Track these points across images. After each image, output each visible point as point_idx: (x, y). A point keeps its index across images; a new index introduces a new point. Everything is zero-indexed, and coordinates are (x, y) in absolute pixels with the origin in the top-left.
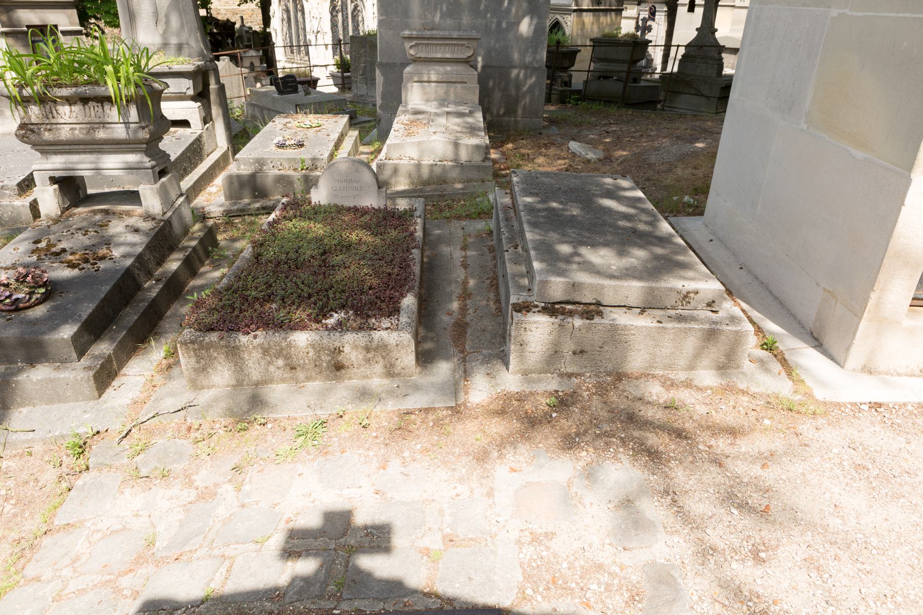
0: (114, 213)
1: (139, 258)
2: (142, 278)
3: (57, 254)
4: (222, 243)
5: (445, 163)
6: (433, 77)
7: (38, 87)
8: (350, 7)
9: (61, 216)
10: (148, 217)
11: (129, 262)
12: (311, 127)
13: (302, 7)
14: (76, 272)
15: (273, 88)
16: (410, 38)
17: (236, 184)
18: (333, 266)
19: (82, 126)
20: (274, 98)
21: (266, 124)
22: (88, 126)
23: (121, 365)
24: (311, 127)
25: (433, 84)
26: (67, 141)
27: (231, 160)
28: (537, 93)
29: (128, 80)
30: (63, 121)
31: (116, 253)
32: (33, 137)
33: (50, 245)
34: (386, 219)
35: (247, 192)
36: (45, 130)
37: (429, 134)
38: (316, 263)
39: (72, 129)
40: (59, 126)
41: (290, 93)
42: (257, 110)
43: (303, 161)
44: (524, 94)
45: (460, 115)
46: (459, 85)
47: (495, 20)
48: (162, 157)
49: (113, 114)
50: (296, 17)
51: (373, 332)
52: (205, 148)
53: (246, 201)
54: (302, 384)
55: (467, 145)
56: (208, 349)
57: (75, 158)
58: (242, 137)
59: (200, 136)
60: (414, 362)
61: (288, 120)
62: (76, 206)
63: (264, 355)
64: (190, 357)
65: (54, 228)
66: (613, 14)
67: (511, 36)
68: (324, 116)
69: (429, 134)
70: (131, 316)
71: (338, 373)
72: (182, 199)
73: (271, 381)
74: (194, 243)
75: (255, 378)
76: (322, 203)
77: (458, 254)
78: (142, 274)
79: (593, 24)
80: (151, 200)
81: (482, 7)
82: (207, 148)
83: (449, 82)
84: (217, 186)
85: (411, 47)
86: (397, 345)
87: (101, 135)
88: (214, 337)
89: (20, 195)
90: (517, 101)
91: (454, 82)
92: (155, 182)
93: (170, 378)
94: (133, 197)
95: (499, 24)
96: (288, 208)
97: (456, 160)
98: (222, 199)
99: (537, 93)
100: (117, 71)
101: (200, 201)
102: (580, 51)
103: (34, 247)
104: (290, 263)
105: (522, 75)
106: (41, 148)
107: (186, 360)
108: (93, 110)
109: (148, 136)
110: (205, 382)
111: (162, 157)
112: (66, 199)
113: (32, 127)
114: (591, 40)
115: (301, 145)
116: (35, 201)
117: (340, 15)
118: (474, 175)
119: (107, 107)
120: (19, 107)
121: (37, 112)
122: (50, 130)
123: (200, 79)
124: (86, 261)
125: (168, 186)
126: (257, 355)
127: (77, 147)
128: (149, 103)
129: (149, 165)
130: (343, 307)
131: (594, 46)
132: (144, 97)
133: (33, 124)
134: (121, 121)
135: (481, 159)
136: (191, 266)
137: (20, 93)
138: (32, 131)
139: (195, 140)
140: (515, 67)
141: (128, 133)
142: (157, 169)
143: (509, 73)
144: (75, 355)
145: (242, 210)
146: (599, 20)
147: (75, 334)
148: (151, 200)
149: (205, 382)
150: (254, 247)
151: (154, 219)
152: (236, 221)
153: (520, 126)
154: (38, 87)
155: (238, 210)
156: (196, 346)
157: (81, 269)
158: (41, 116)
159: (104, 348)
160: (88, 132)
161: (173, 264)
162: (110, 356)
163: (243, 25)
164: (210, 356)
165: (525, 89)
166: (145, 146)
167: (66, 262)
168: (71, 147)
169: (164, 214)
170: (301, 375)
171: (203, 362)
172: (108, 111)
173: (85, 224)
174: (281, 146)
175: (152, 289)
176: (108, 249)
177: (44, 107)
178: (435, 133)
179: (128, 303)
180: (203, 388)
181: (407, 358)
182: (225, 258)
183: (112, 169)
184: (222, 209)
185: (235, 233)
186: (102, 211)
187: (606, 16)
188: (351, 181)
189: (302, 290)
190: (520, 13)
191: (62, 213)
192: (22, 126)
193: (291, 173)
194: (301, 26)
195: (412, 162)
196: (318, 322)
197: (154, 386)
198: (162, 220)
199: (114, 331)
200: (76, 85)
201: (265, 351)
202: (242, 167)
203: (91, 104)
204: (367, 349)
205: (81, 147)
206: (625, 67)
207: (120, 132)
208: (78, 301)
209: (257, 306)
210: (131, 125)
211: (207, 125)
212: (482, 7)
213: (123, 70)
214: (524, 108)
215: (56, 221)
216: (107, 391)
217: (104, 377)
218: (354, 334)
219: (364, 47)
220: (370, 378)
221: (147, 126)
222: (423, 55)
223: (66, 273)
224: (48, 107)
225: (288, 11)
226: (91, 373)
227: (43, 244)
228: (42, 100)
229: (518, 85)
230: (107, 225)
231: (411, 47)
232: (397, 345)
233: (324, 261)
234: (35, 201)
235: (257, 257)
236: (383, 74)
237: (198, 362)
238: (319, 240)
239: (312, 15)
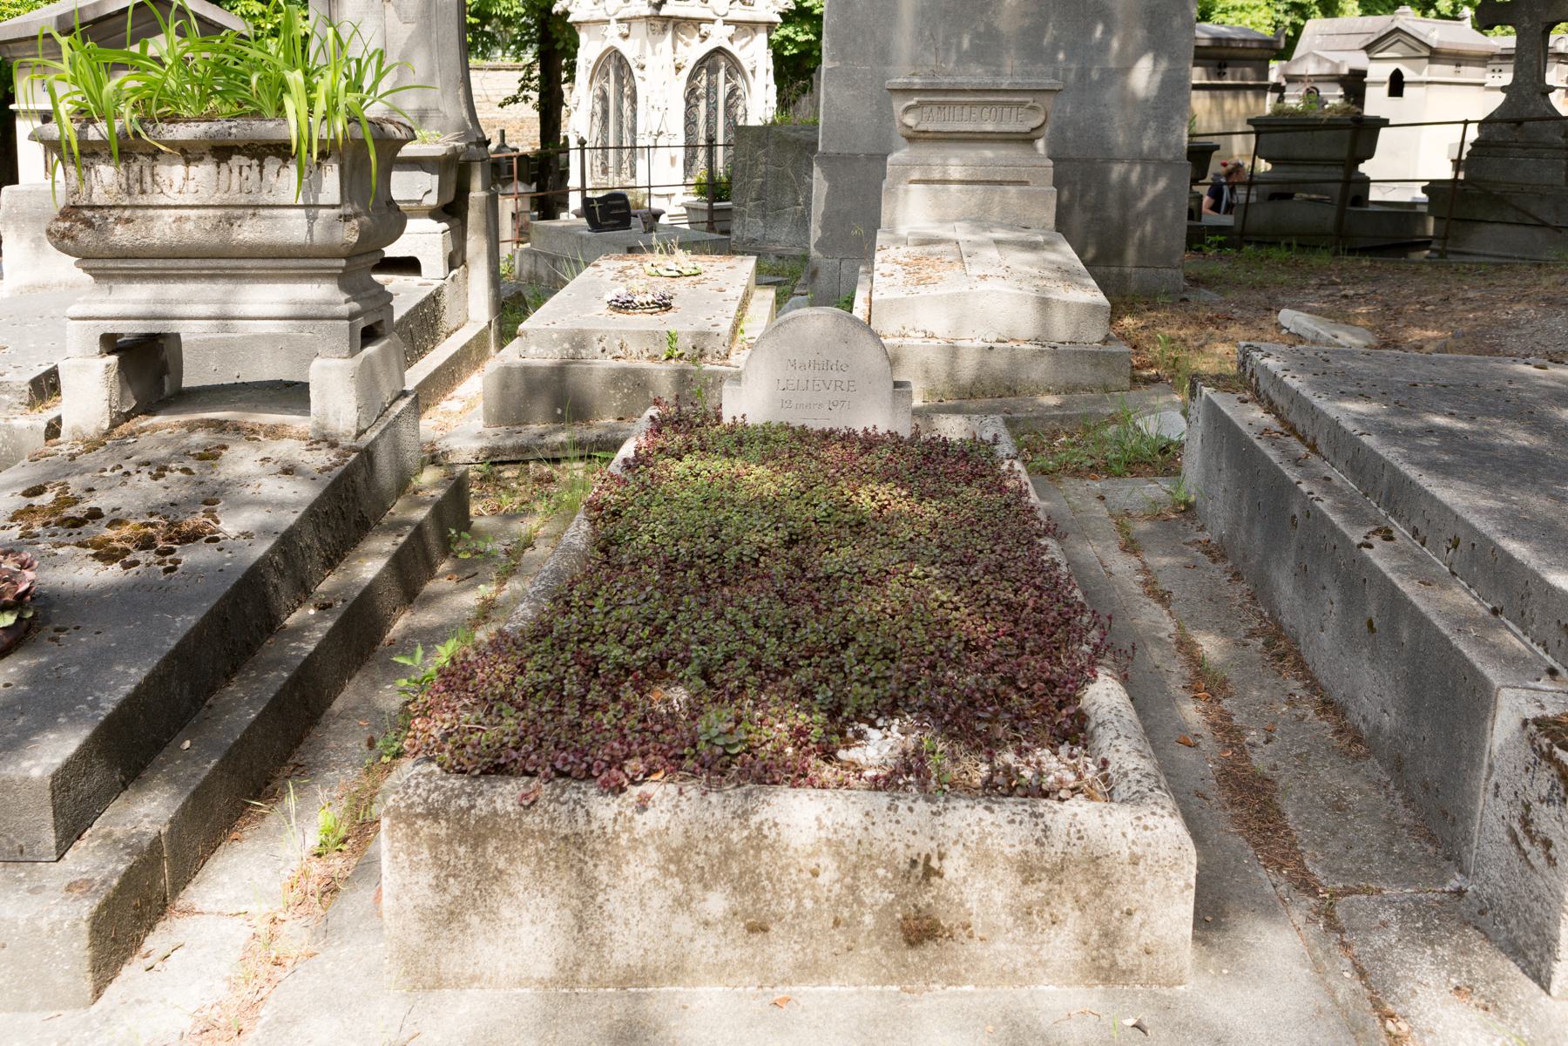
0: (238, 429)
1: (287, 541)
2: (284, 598)
3: (77, 523)
4: (478, 522)
5: (1014, 345)
6: (955, 172)
7: (127, 118)
8: (723, 91)
9: (107, 434)
10: (325, 439)
11: (261, 549)
12: (681, 275)
13: (634, 90)
14: (113, 573)
15: (584, 221)
16: (907, 91)
17: (517, 387)
18: (828, 577)
19: (203, 212)
20: (581, 237)
21: (579, 271)
22: (219, 212)
23: (185, 874)
24: (681, 275)
25: (953, 187)
26: (163, 247)
27: (492, 349)
28: (1170, 213)
29: (333, 108)
30: (163, 200)
31: (230, 525)
32: (86, 237)
33: (65, 501)
34: (924, 463)
35: (540, 406)
36: (118, 220)
37: (963, 286)
38: (778, 569)
39: (180, 219)
40: (151, 212)
41: (614, 228)
42: (542, 261)
43: (672, 338)
44: (1140, 218)
45: (1033, 246)
46: (1012, 189)
47: (1073, 66)
48: (374, 297)
49: (285, 182)
50: (619, 109)
51: (1043, 805)
52: (445, 318)
53: (535, 428)
54: (781, 991)
55: (1067, 305)
56: (478, 841)
57: (176, 290)
58: (513, 311)
59: (439, 291)
60: (1188, 931)
61: (627, 264)
62: (150, 412)
63: (665, 872)
64: (415, 867)
65: (85, 460)
66: (1250, 94)
67: (1110, 95)
68: (704, 258)
69: (963, 286)
70: (242, 705)
71: (912, 956)
72: (403, 404)
73: (677, 971)
74: (421, 514)
75: (619, 958)
76: (749, 422)
77: (1122, 565)
78: (285, 588)
79: (1210, 112)
80: (336, 396)
81: (1047, 40)
82: (448, 319)
83: (989, 182)
84: (474, 390)
85: (907, 110)
86: (1135, 861)
87: (249, 232)
88: (505, 795)
89: (31, 405)
90: (1123, 232)
91: (1000, 183)
92: (352, 354)
93: (326, 931)
94: (293, 394)
95: (1083, 74)
96: (666, 430)
97: (951, 376)
98: (478, 424)
99: (1170, 213)
100: (310, 88)
101: (430, 425)
102: (1217, 147)
103: (22, 503)
104: (706, 566)
105: (1134, 177)
106: (99, 264)
107: (401, 873)
108: (238, 177)
109: (355, 239)
110: (452, 963)
111: (374, 297)
112: (129, 394)
113: (88, 214)
114: (1250, 122)
115: (664, 305)
116: (59, 420)
117: (703, 104)
118: (1085, 374)
119: (272, 165)
120: (71, 169)
121: (107, 181)
122: (128, 221)
123: (453, 176)
124: (146, 543)
125: (379, 368)
126: (641, 869)
127: (181, 263)
128: (373, 157)
129: (344, 309)
130: (892, 709)
131: (1258, 134)
132: (363, 142)
133: (92, 207)
134: (301, 202)
135: (1100, 336)
136: (409, 573)
137: (81, 133)
138: (89, 224)
139: (427, 299)
140: (1120, 160)
141: (310, 231)
142: (362, 323)
143: (1106, 173)
144: (49, 838)
145: (525, 449)
146: (1221, 107)
147: (68, 765)
148: (336, 396)
149: (452, 963)
150: (593, 522)
151: (333, 445)
152: (507, 474)
153: (1133, 286)
154: (127, 118)
155: (514, 449)
156: (442, 829)
157: (126, 566)
158: (115, 189)
159: (149, 811)
160: (215, 228)
161: (369, 566)
162: (156, 842)
163: (503, 145)
164: (481, 867)
165: (1142, 205)
166: (343, 263)
167: (93, 545)
168: (169, 263)
169: (360, 433)
170: (782, 951)
171: (455, 887)
172: (273, 179)
173: (163, 452)
174: (623, 306)
175: (309, 626)
176: (210, 513)
177: (127, 168)
178: (984, 277)
179: (235, 669)
180: (439, 983)
181: (1170, 912)
182: (489, 557)
183: (246, 323)
184: (477, 445)
185: (508, 503)
186: (209, 424)
187: (1236, 97)
188: (827, 366)
189: (761, 647)
190: (1130, 49)
191: (114, 425)
192: (70, 211)
193: (645, 364)
194: (627, 123)
195: (933, 342)
196: (828, 756)
197: (277, 963)
198: (353, 449)
199: (186, 757)
200: (209, 119)
201: (675, 860)
202: (532, 350)
203: (236, 160)
204: (1028, 871)
205: (193, 263)
206: (1338, 173)
207: (293, 228)
208: (101, 660)
209: (628, 693)
210: (322, 212)
211: (455, 272)
212: (1047, 40)
213: (323, 86)
214: (1142, 244)
215: (93, 445)
216: (126, 971)
217: (128, 918)
218: (980, 811)
219: (764, 146)
220: (1022, 982)
221: (356, 216)
222: (931, 127)
223: (82, 573)
224: (135, 167)
225: (604, 98)
226: (87, 907)
227: (47, 499)
228: (127, 150)
229: (1127, 197)
230: (216, 457)
231: (907, 110)
232: (1135, 861)
233: (798, 562)
234: (59, 420)
235: (606, 546)
236: (829, 176)
237: (440, 888)
238: (770, 506)
239: (651, 102)
